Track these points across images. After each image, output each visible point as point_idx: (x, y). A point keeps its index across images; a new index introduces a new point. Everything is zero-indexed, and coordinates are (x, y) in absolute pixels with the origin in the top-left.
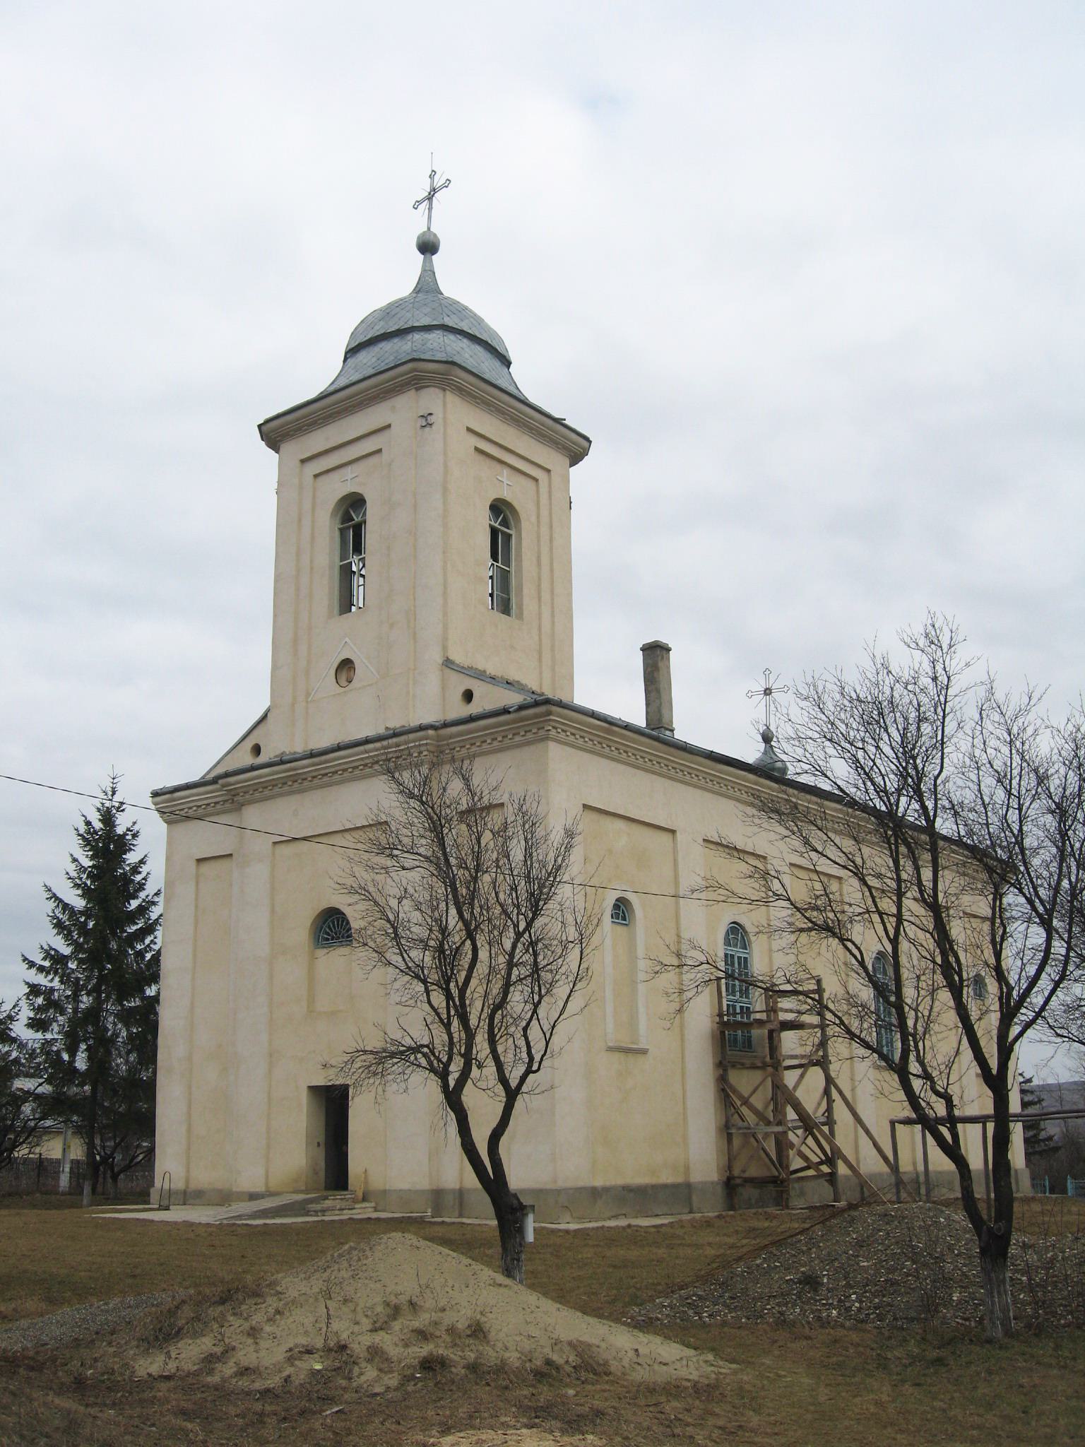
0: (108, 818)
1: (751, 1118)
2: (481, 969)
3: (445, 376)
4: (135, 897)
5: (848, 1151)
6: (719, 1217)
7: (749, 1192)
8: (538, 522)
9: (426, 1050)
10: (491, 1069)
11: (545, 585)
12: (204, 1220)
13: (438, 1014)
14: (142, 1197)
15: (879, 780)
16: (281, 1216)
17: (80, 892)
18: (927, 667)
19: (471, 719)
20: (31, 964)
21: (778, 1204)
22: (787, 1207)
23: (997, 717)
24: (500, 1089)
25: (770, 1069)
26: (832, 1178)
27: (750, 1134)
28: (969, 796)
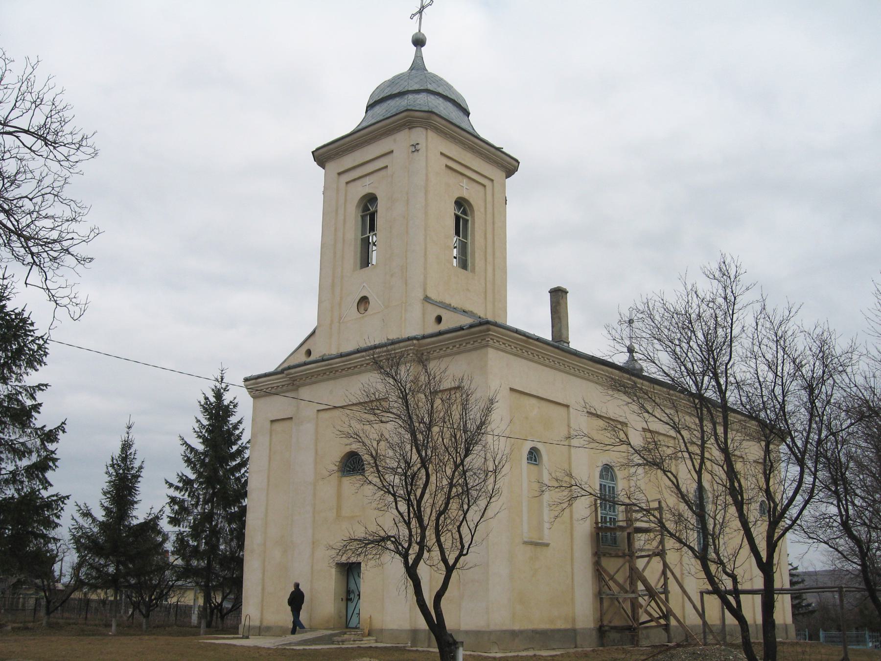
0: (218, 395)
1: (615, 588)
2: (432, 487)
3: (426, 120)
4: (235, 444)
5: (677, 611)
6: (593, 651)
7: (613, 635)
8: (486, 211)
9: (393, 539)
10: (436, 553)
11: (490, 250)
12: (267, 645)
13: (402, 517)
14: (233, 630)
15: (689, 365)
16: (316, 644)
17: (201, 440)
18: (721, 291)
19: (440, 333)
20: (171, 485)
21: (632, 644)
22: (637, 645)
23: (768, 325)
24: (442, 565)
25: (627, 558)
26: (667, 627)
27: (614, 599)
28: (749, 377)
